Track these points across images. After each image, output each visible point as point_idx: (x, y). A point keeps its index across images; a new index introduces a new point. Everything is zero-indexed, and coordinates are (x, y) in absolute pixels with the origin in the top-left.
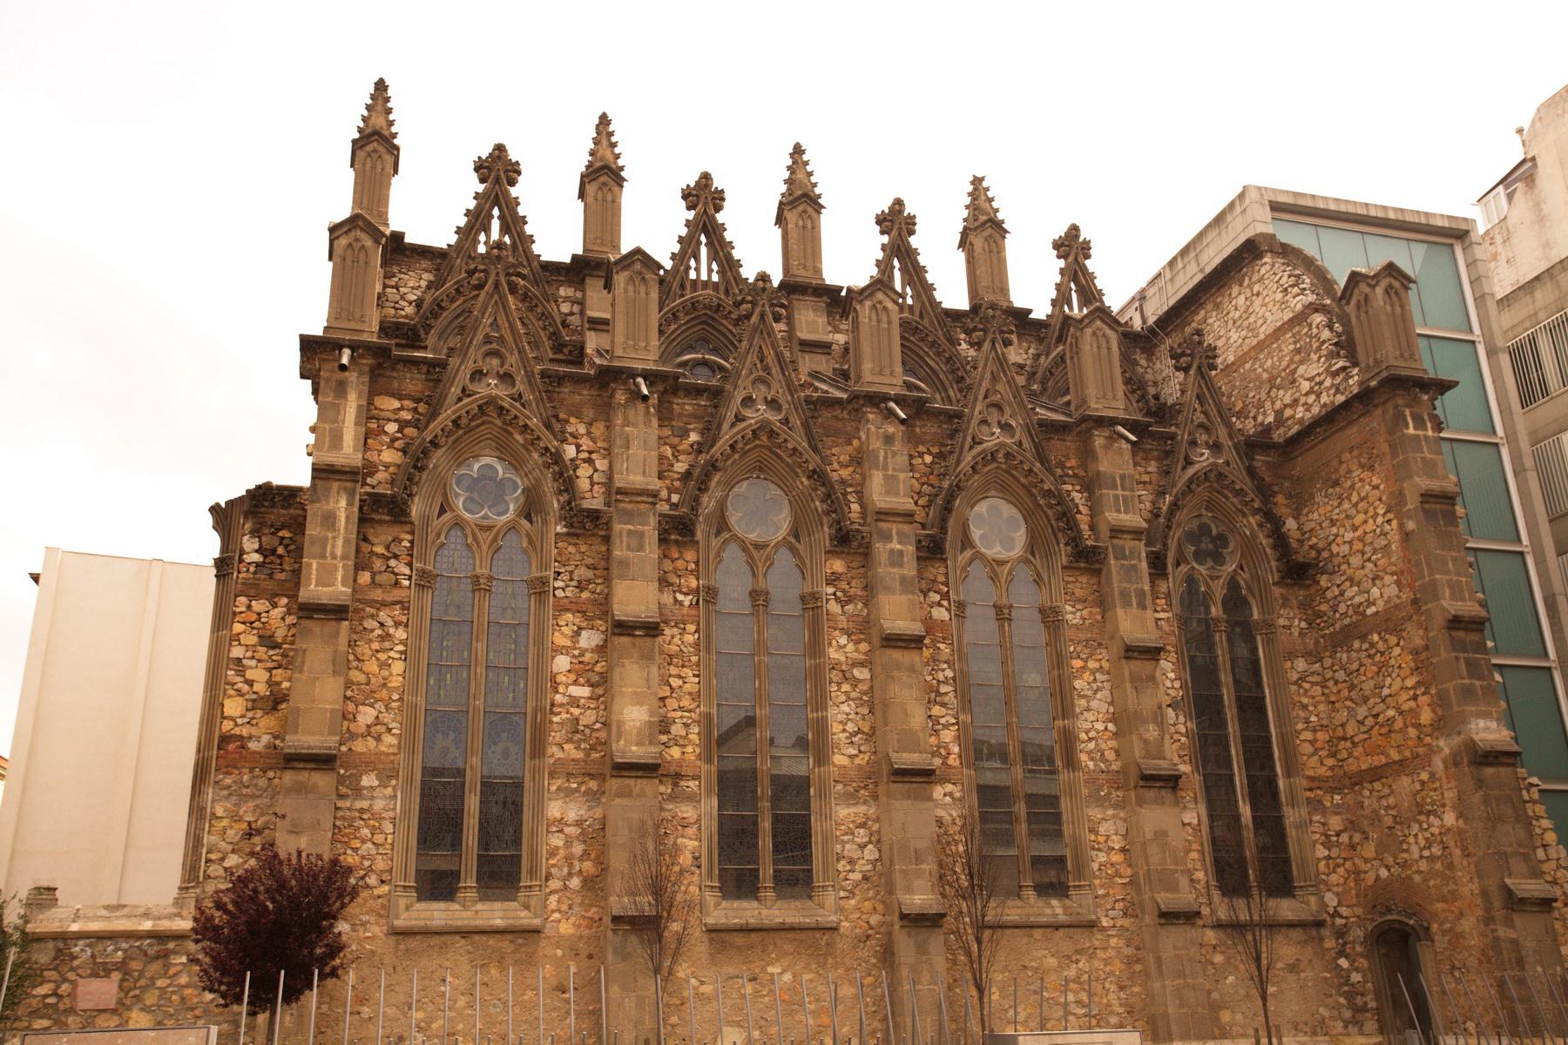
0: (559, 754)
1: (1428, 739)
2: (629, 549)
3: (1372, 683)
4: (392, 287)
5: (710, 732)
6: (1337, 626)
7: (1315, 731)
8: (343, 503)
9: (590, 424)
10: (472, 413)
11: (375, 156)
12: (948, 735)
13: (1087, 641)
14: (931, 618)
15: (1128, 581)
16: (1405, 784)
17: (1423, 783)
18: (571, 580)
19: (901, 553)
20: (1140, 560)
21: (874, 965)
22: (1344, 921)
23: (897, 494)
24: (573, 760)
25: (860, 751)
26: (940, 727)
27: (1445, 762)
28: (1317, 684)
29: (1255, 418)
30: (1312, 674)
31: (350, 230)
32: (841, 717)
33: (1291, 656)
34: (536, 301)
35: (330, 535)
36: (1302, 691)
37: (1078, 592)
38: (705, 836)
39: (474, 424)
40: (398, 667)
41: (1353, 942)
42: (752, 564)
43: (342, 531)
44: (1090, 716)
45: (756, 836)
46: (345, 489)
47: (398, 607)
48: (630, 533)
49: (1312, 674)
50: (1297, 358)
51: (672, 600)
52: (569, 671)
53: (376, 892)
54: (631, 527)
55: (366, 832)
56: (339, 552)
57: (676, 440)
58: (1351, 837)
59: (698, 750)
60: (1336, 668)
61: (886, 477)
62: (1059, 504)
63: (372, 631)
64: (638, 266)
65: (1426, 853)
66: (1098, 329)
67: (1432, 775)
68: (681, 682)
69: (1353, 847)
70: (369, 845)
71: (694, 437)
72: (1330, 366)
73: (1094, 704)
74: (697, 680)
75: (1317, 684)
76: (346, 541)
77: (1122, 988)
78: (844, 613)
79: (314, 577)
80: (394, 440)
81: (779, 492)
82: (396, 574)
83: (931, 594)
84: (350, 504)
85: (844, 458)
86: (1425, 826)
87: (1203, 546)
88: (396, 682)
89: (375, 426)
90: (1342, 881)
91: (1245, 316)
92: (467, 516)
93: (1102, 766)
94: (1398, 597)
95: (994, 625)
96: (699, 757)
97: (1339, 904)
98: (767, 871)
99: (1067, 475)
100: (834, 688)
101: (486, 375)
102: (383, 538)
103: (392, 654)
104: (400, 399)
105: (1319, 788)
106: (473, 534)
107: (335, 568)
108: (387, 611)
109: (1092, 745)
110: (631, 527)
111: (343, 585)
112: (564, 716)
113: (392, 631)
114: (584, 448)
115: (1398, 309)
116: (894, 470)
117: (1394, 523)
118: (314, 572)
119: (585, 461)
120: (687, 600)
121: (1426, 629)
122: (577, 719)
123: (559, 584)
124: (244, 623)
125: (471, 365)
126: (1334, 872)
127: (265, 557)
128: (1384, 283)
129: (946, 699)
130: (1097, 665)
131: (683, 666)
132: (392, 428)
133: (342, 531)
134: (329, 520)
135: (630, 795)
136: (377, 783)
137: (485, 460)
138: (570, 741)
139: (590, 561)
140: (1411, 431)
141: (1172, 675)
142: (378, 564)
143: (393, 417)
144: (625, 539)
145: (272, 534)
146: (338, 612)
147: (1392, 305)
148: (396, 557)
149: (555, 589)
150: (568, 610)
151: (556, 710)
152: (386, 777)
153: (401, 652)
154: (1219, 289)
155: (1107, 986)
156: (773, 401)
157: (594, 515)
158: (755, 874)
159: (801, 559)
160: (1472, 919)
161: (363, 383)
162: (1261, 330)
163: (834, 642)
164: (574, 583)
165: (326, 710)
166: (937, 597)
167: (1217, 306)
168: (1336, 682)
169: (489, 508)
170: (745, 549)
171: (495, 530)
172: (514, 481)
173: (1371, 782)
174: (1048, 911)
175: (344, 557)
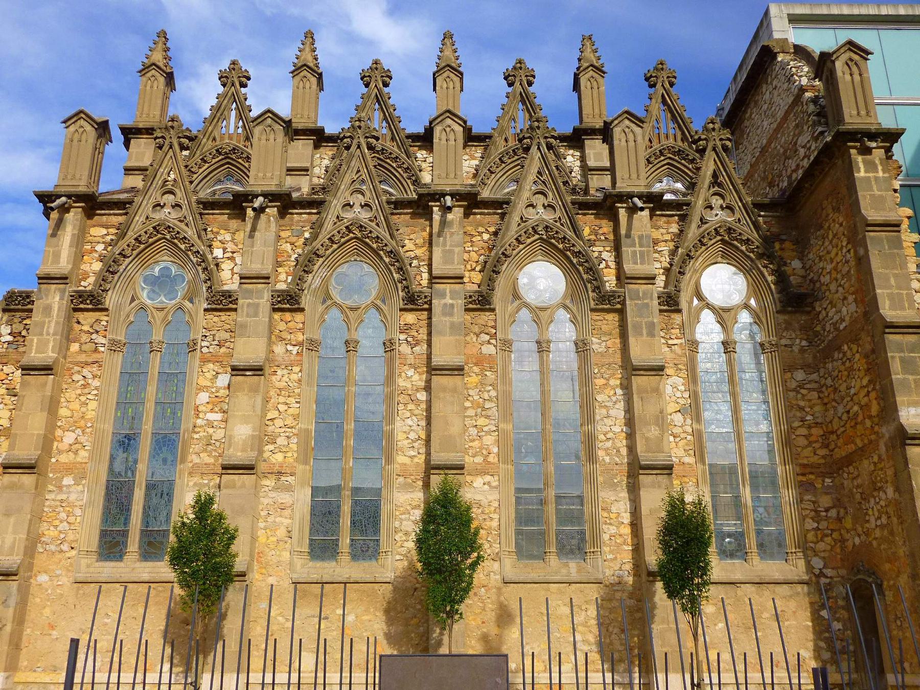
0: (197, 460)
1: (876, 428)
2: (248, 315)
3: (845, 385)
5: (307, 443)
6: (826, 342)
7: (810, 427)
8: (57, 298)
9: (234, 233)
10: (149, 232)
11: (153, 79)
12: (489, 440)
13: (610, 364)
14: (481, 353)
15: (641, 316)
16: (866, 465)
17: (875, 464)
19: (452, 306)
20: (652, 299)
21: (419, 610)
22: (828, 581)
24: (206, 464)
25: (419, 453)
26: (483, 433)
27: (886, 445)
28: (814, 390)
29: (778, 185)
30: (810, 382)
31: (77, 121)
32: (407, 429)
36: (799, 396)
37: (605, 328)
38: (297, 516)
40: (93, 405)
41: (836, 598)
42: (347, 321)
43: (55, 317)
44: (608, 422)
45: (339, 516)
48: (249, 305)
49: (810, 382)
50: (797, 132)
52: (208, 403)
53: (68, 555)
55: (63, 515)
56: (51, 331)
58: (838, 512)
59: (295, 455)
60: (826, 376)
61: (444, 251)
63: (78, 381)
65: (879, 523)
67: (880, 457)
68: (286, 408)
69: (839, 519)
70: (65, 524)
72: (814, 133)
73: (612, 412)
74: (298, 405)
75: (814, 390)
76: (57, 323)
77: (623, 631)
79: (34, 348)
81: (372, 270)
82: (96, 344)
83: (483, 335)
84: (62, 299)
86: (877, 500)
88: (91, 415)
89: (90, 247)
90: (829, 548)
91: (770, 106)
92: (149, 302)
93: (617, 459)
94: (856, 312)
95: (536, 356)
96: (296, 460)
97: (825, 567)
98: (345, 542)
99: (600, 240)
100: (401, 407)
102: (89, 320)
103: (90, 397)
104: (107, 228)
105: (812, 473)
106: (152, 313)
107: (48, 341)
108: (89, 369)
109: (609, 444)
110: (251, 301)
112: (202, 434)
113: (90, 381)
114: (229, 250)
115: (857, 78)
116: (451, 246)
117: (852, 251)
118: (35, 345)
120: (295, 350)
121: (873, 336)
122: (211, 436)
123: (205, 344)
125: (152, 200)
126: (822, 540)
127: (15, 337)
128: (844, 57)
129: (489, 413)
131: (289, 396)
132: (100, 248)
133: (55, 317)
134: (48, 309)
135: (234, 487)
136: (73, 482)
137: (162, 265)
138: (205, 451)
140: (862, 174)
141: (682, 388)
143: (101, 240)
145: (20, 322)
146: (47, 369)
147: (851, 75)
148: (97, 332)
149: (202, 347)
150: (209, 361)
151: (197, 430)
152: (80, 478)
153: (96, 395)
154: (755, 91)
155: (611, 629)
156: (366, 205)
157: (228, 295)
158: (336, 543)
159: (385, 316)
160: (905, 576)
161: (77, 220)
162: (779, 114)
163: (403, 374)
164: (216, 342)
165: (33, 434)
167: (756, 102)
168: (827, 387)
169: (165, 296)
170: (342, 311)
172: (182, 276)
173: (847, 467)
174: (564, 571)
175: (55, 334)
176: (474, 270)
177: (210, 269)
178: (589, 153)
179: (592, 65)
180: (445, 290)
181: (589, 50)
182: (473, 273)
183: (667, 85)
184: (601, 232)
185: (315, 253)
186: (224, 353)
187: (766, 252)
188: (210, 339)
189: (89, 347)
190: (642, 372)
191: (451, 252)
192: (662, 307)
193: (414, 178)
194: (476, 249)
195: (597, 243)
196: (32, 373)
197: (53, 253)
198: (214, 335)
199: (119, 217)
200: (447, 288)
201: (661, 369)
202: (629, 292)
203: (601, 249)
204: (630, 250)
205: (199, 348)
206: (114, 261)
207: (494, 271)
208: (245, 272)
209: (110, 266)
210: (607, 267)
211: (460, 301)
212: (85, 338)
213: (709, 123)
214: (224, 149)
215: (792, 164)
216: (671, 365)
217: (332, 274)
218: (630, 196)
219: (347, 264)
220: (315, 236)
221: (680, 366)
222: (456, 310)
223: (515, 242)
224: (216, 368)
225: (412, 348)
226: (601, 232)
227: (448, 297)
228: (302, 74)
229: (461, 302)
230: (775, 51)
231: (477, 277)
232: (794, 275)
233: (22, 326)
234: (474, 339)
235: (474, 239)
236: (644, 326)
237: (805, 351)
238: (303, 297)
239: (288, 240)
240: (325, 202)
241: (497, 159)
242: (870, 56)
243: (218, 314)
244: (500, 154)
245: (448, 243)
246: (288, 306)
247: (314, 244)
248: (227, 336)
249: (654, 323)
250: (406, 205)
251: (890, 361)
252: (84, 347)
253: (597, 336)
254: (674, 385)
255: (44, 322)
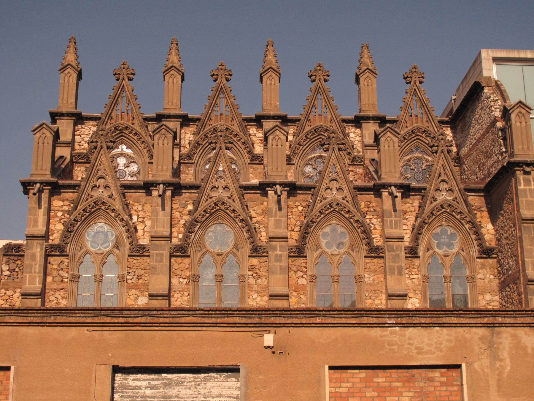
2: (156, 261)
4: (78, 135)
8: (39, 249)
9: (144, 205)
13: (375, 291)
15: (394, 262)
18: (134, 275)
19: (281, 255)
20: (401, 251)
23: (280, 228)
31: (40, 130)
33: (483, 292)
34: (140, 136)
35: (34, 263)
37: (372, 268)
39: (92, 210)
43: (38, 261)
46: (39, 243)
47: (63, 291)
48: (157, 254)
51: (177, 282)
54: (158, 252)
56: (37, 270)
57: (182, 209)
61: (276, 221)
62: (362, 226)
63: (53, 301)
64: (163, 131)
66: (389, 137)
71: (190, 207)
76: (40, 265)
78: (256, 284)
79: (27, 281)
80: (61, 219)
81: (230, 229)
82: (62, 277)
83: (299, 272)
84: (41, 249)
85: (259, 211)
87: (442, 240)
99: (371, 211)
101: (98, 188)
108: (59, 292)
110: (158, 252)
111: (39, 284)
113: (60, 301)
114: (141, 216)
115: (524, 124)
116: (279, 217)
118: (28, 279)
119: (141, 222)
123: (129, 277)
124: (4, 300)
127: (11, 272)
130: (379, 302)
132: (60, 214)
133: (38, 261)
134: (33, 256)
139: (143, 266)
140: (522, 187)
142: (55, 273)
144: (155, 257)
148: (62, 269)
149: (127, 280)
150: (133, 288)
157: (143, 247)
159: (239, 259)
163: (251, 297)
164: (136, 277)
166: (301, 274)
171: (103, 255)
175: (39, 272)
176: (293, 230)
177: (132, 230)
178: (365, 133)
179: (368, 69)
180: (276, 245)
181: (366, 56)
182: (293, 232)
183: (418, 83)
184: (371, 205)
185: (196, 221)
186: (142, 283)
187: (471, 221)
188: (132, 274)
189: (58, 279)
190: (394, 298)
191: (279, 221)
192: (408, 255)
193: (248, 149)
194: (294, 217)
195: (369, 213)
196: (28, 297)
197: (33, 219)
198: (134, 272)
199: (71, 194)
200: (278, 244)
201: (406, 296)
202: (387, 247)
203: (371, 217)
204: (389, 219)
205: (126, 279)
206: (71, 225)
207: (305, 233)
208: (153, 234)
209: (69, 228)
210: (375, 228)
211: (286, 253)
212: (55, 273)
213: (440, 135)
214: (119, 127)
215: (490, 162)
216: (412, 291)
217: (205, 232)
218: (390, 185)
219: (215, 225)
220: (196, 209)
221: (417, 292)
222: (283, 258)
223: (319, 214)
224: (137, 293)
225: (256, 280)
226: (371, 205)
227: (278, 250)
228: (171, 73)
229: (286, 253)
230: (483, 85)
231: (296, 235)
232: (488, 233)
233: (15, 265)
234: (294, 275)
235: (293, 210)
236: (396, 268)
237: (491, 282)
238: (189, 249)
239: (178, 210)
240: (201, 186)
241: (304, 137)
242: (531, 111)
243: (136, 258)
244: (305, 133)
245: (278, 215)
246: (180, 254)
247: (195, 215)
248: (142, 272)
249: (402, 266)
250: (251, 188)
251: (529, 301)
252: (56, 279)
253: (368, 273)
254: (413, 304)
255: (32, 265)
